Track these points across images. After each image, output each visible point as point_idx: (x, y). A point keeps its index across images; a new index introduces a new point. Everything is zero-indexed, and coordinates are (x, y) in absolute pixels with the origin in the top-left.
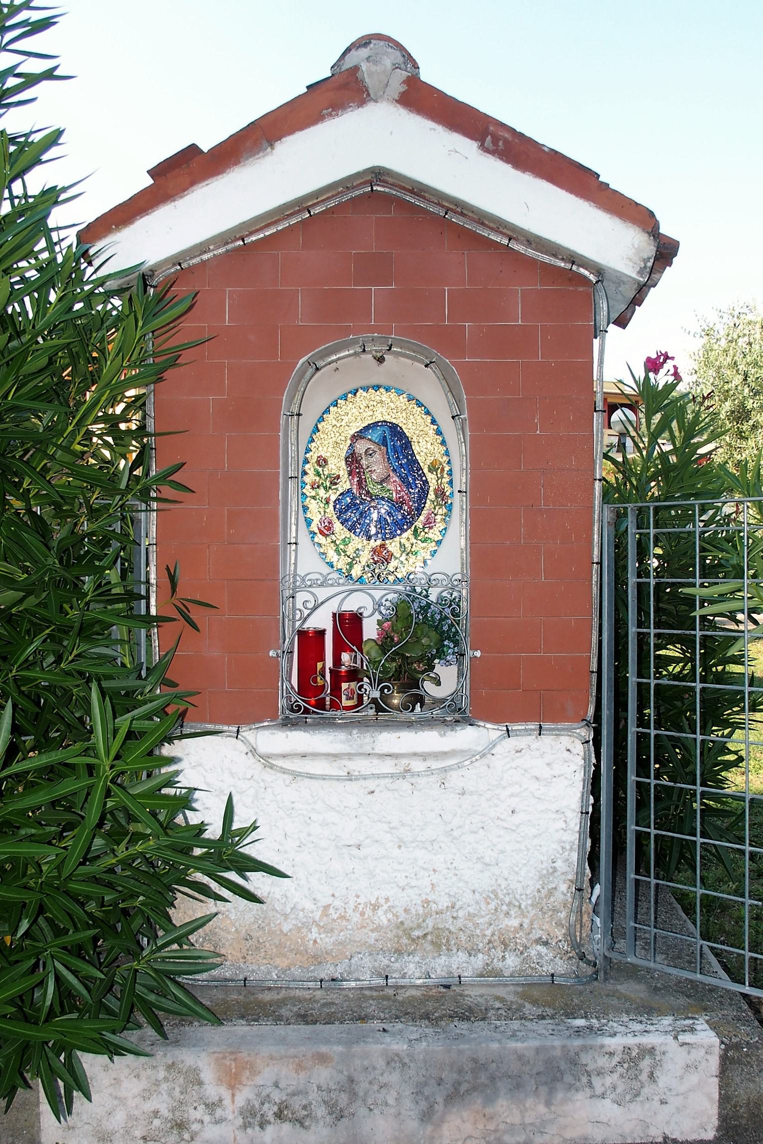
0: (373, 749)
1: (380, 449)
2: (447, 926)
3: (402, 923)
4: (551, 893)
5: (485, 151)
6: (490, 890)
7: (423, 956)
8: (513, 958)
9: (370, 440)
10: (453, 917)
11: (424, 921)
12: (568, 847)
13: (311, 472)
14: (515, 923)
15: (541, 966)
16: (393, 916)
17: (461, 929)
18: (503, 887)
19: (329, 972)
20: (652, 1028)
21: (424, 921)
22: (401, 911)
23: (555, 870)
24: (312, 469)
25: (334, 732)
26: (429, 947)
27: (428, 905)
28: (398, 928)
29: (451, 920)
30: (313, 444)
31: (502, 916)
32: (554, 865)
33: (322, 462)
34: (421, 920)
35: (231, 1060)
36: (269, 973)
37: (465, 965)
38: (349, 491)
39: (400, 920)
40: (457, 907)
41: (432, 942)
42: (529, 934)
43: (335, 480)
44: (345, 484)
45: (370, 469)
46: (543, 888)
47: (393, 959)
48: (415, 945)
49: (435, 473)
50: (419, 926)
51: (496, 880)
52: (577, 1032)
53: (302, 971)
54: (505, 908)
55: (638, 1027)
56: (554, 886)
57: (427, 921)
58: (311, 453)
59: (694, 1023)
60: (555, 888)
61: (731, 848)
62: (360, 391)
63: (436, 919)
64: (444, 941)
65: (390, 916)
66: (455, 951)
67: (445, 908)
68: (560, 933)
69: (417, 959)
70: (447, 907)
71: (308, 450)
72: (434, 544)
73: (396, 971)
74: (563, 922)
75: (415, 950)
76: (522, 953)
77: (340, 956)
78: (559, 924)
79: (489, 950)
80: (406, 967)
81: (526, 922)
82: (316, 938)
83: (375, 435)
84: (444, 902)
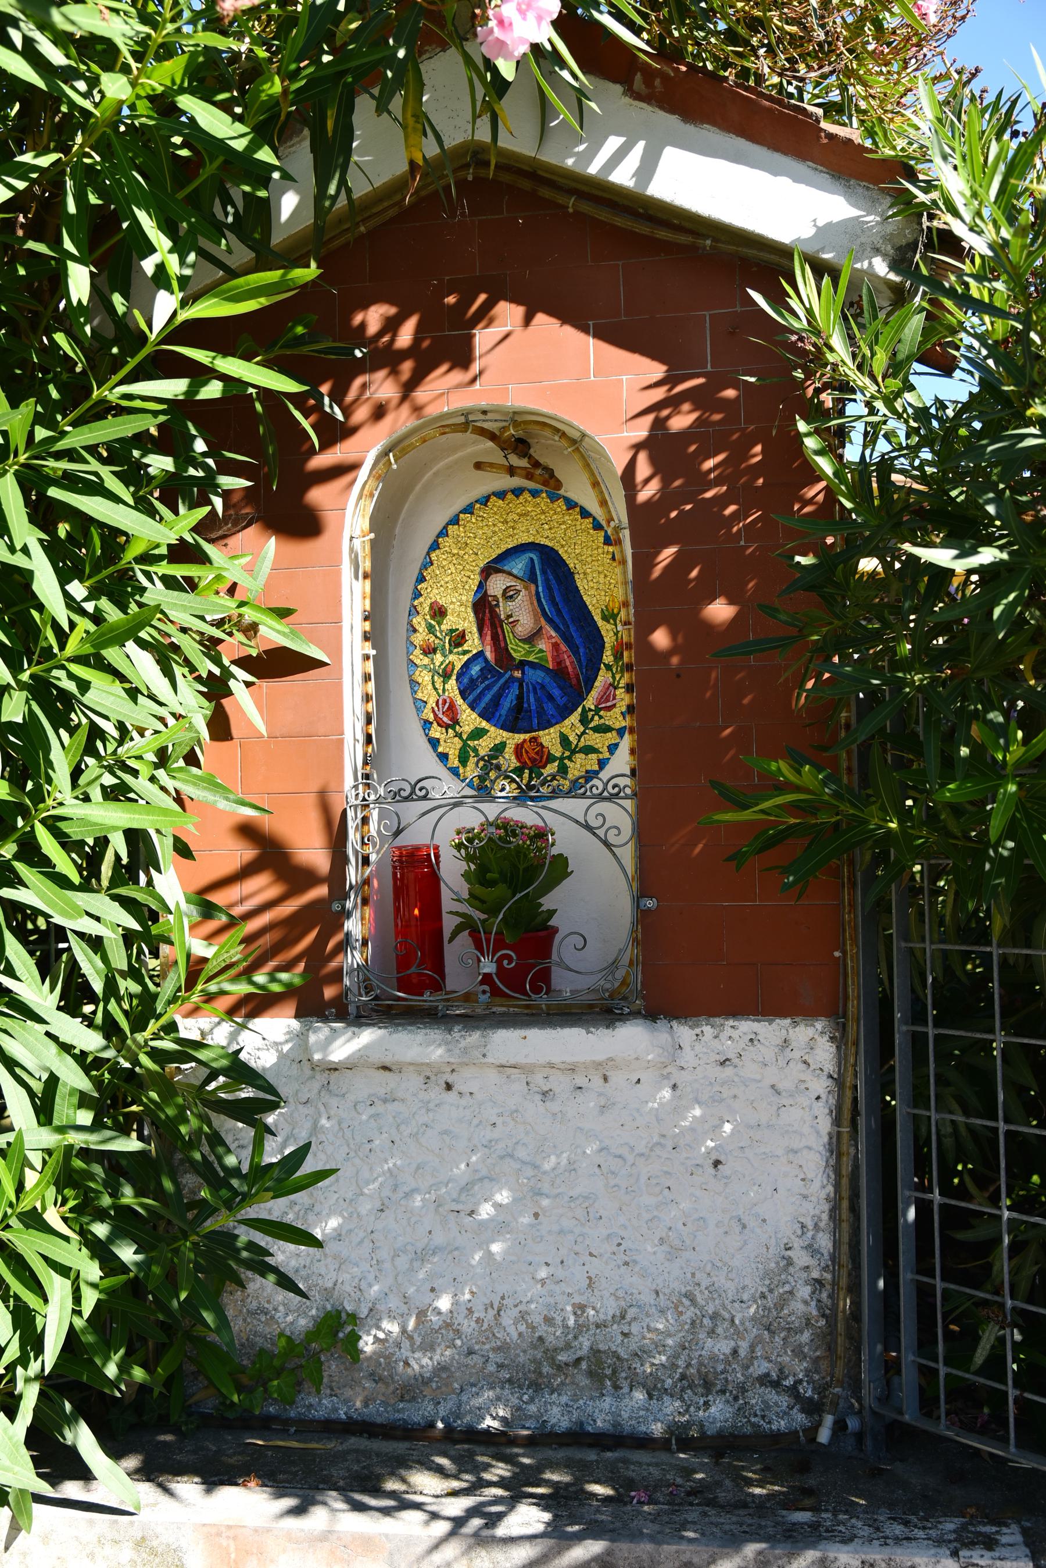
0: (484, 1056)
1: (526, 588)
2: (614, 1348)
3: (541, 1339)
4: (782, 1302)
5: (635, 99)
6: (683, 1291)
7: (575, 1395)
8: (721, 1406)
9: (510, 574)
10: (622, 1333)
11: (575, 1338)
12: (810, 1225)
13: (422, 628)
14: (724, 1347)
15: (769, 1423)
16: (527, 1327)
17: (637, 1354)
18: (703, 1287)
19: (426, 1413)
20: (921, 1534)
21: (575, 1338)
22: (537, 1319)
23: (790, 1262)
24: (423, 624)
25: (425, 1028)
26: (584, 1381)
27: (584, 1312)
28: (534, 1347)
29: (620, 1338)
30: (423, 585)
31: (702, 1336)
32: (789, 1253)
33: (439, 612)
34: (570, 1336)
35: (228, 1537)
36: (335, 1410)
37: (642, 1413)
38: (480, 654)
39: (537, 1335)
40: (628, 1317)
41: (590, 1374)
42: (748, 1367)
43: (458, 639)
44: (473, 644)
45: (511, 620)
46: (771, 1291)
47: (526, 1397)
48: (563, 1377)
49: (612, 621)
50: (568, 1346)
51: (693, 1275)
52: (789, 1531)
53: (386, 1410)
54: (706, 1321)
55: (898, 1529)
56: (787, 1288)
57: (581, 1339)
58: (421, 599)
59: (997, 1532)
60: (791, 1292)
61: (1026, 1222)
62: (493, 499)
63: (595, 1335)
64: (608, 1372)
65: (522, 1328)
66: (626, 1390)
67: (610, 1318)
68: (799, 1368)
69: (564, 1399)
70: (614, 1317)
71: (417, 595)
72: (614, 733)
73: (531, 1417)
74: (806, 1350)
75: (562, 1383)
76: (736, 1399)
77: (444, 1389)
78: (798, 1352)
79: (683, 1390)
80: (546, 1411)
81: (744, 1347)
82: (407, 1358)
83: (518, 566)
84: (611, 1308)
